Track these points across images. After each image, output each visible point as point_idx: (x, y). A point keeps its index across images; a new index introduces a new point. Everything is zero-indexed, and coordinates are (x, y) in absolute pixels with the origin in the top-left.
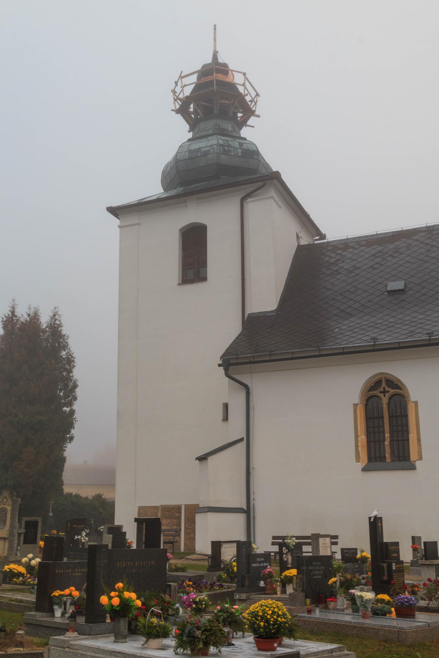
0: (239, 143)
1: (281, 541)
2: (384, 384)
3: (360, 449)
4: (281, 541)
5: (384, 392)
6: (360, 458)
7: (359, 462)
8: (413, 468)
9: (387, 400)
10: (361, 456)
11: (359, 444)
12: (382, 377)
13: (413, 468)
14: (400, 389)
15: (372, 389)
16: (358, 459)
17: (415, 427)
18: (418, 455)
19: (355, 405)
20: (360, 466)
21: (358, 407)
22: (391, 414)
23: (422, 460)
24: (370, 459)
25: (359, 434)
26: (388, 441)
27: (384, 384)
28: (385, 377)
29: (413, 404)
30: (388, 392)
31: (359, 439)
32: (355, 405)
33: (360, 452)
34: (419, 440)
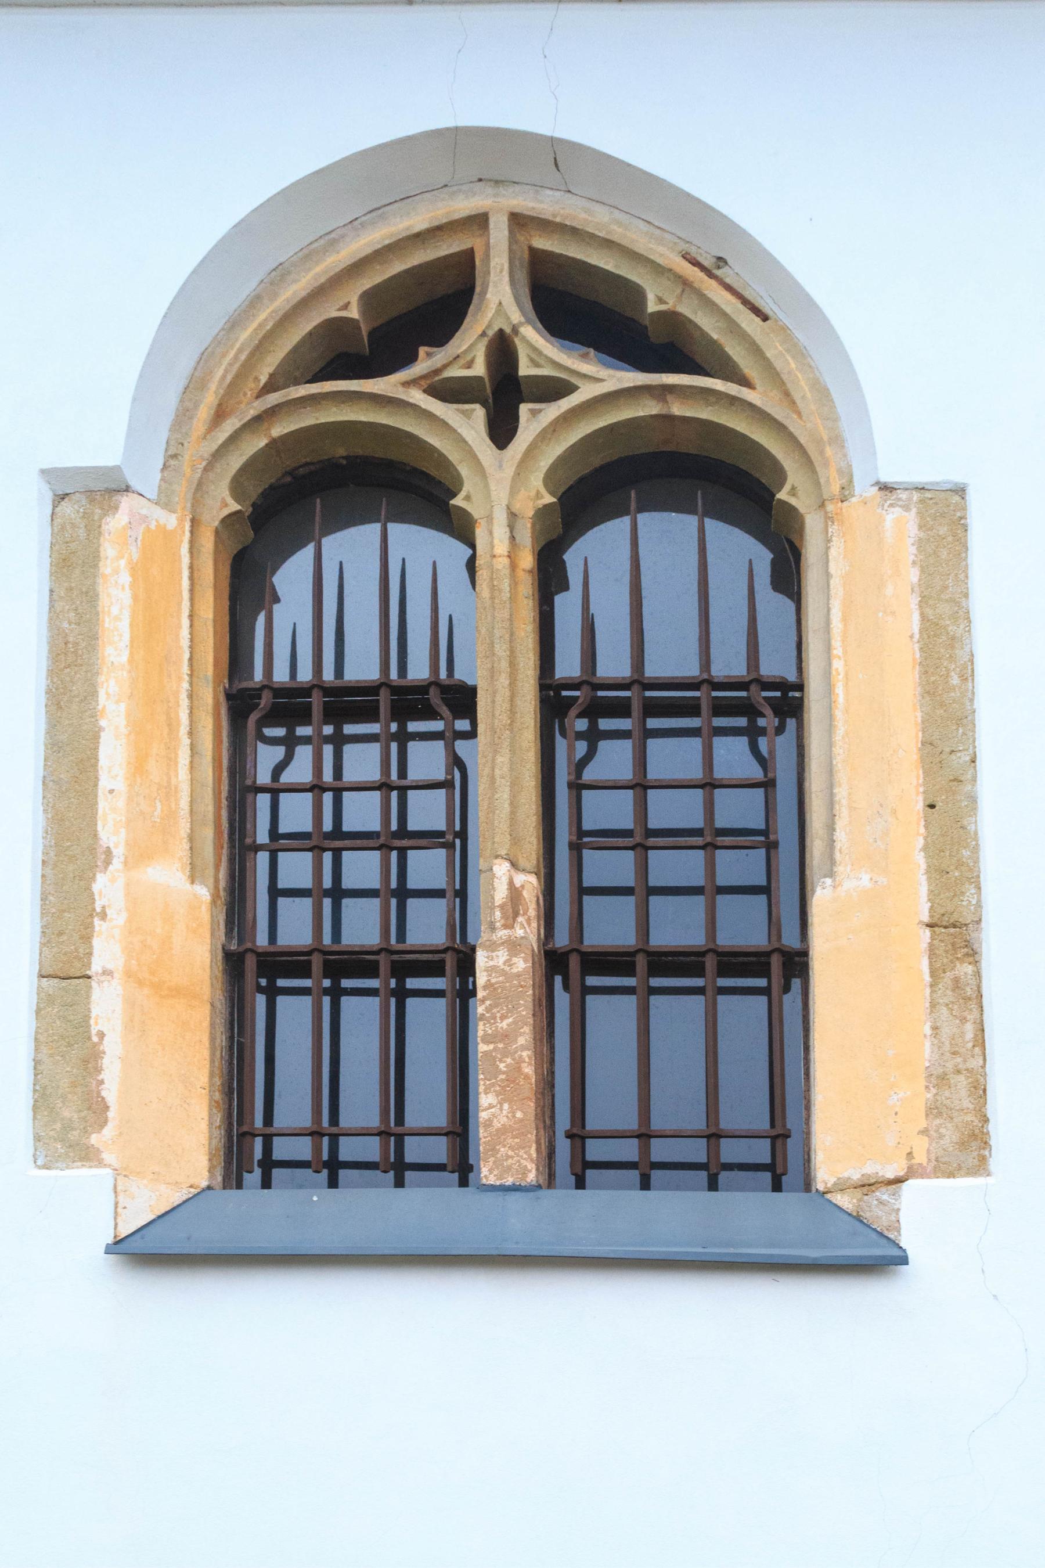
0: (666, 303)
1: (778, 694)
2: (501, 301)
3: (107, 1006)
4: (778, 694)
5: (504, 395)
6: (97, 1110)
7: (88, 1156)
8: (874, 1259)
9: (536, 481)
10: (111, 1092)
11: (107, 951)
12: (480, 221)
13: (874, 1259)
14: (731, 372)
15: (348, 353)
16: (68, 1112)
17: (909, 788)
18: (934, 1110)
19: (85, 497)
20: (95, 1202)
21: (116, 522)
22: (568, 665)
23: (980, 1167)
24: (246, 1150)
25: (112, 831)
26: (513, 946)
27: (501, 301)
28: (518, 221)
29: (900, 525)
30: (552, 389)
31: (108, 888)
32: (85, 497)
33: (113, 1049)
34: (954, 936)
